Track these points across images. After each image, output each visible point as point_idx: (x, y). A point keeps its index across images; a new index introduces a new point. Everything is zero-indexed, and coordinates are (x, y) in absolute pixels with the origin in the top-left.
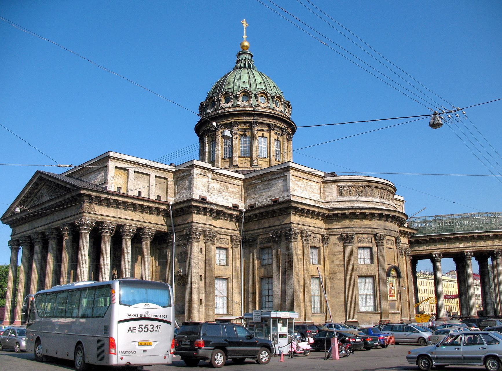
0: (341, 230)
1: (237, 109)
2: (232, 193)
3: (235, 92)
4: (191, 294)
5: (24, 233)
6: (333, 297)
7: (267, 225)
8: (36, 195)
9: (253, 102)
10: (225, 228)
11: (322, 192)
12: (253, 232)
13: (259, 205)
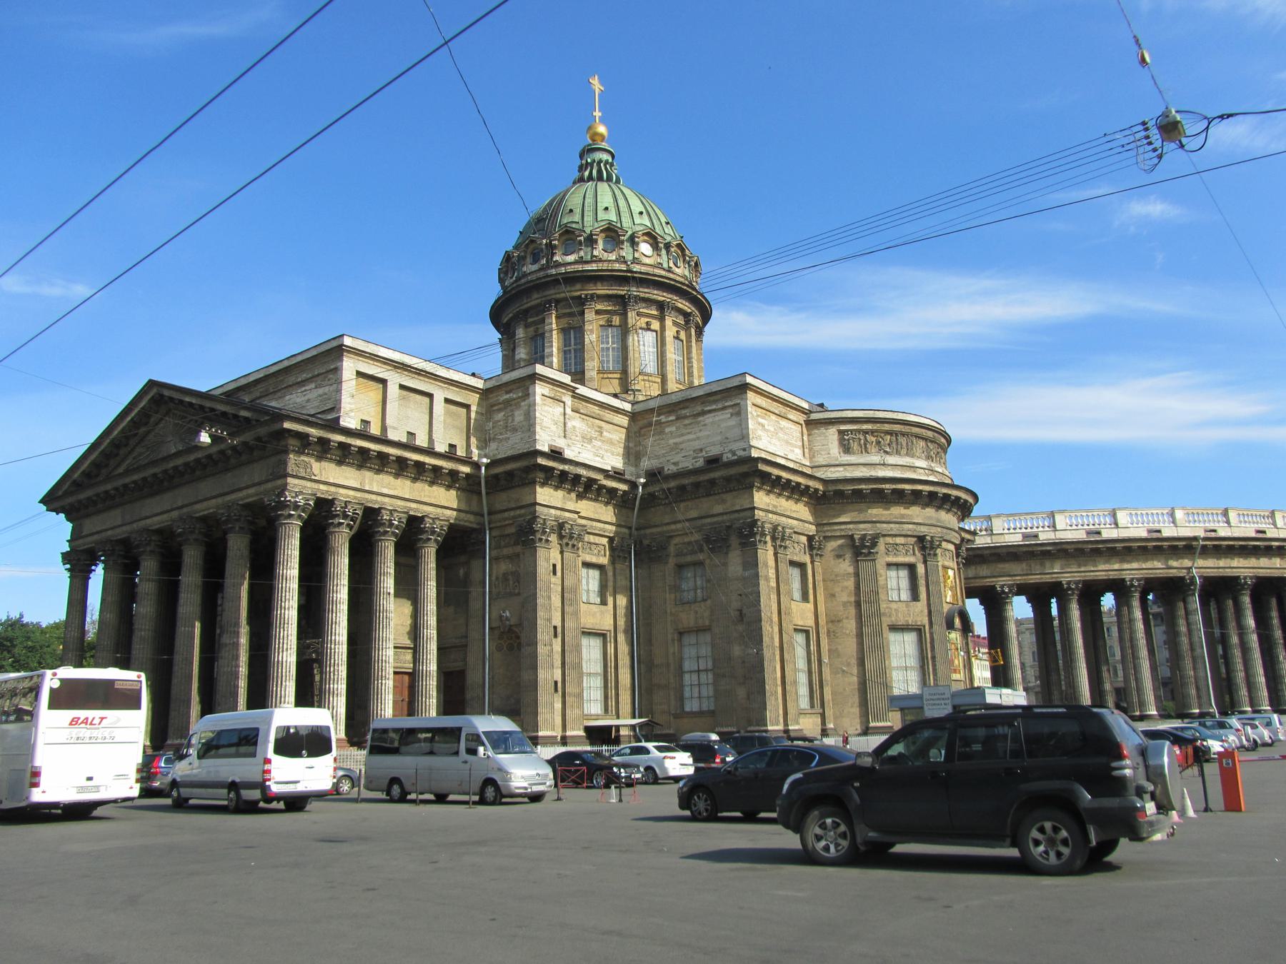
0: (851, 526)
1: (594, 267)
2: (611, 442)
3: (588, 231)
4: (534, 668)
5: (109, 533)
6: (836, 673)
7: (694, 514)
8: (142, 440)
9: (627, 252)
10: (599, 521)
11: (806, 443)
12: (659, 529)
13: (674, 469)
